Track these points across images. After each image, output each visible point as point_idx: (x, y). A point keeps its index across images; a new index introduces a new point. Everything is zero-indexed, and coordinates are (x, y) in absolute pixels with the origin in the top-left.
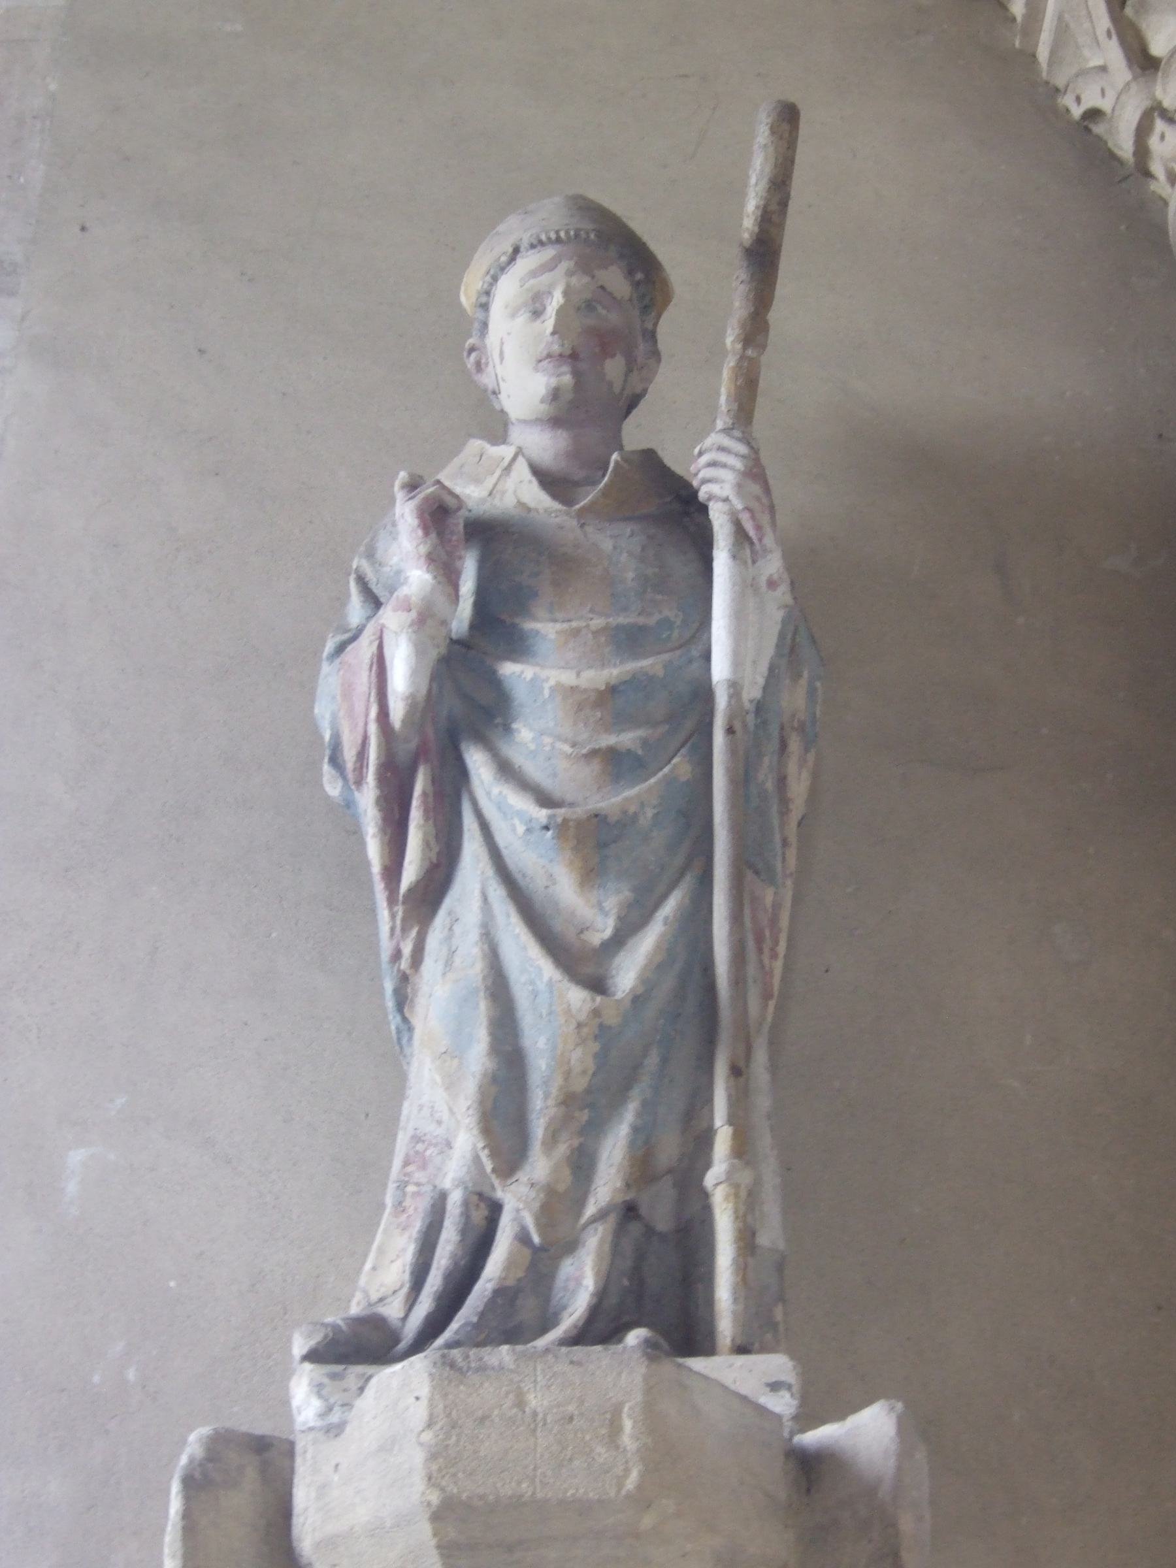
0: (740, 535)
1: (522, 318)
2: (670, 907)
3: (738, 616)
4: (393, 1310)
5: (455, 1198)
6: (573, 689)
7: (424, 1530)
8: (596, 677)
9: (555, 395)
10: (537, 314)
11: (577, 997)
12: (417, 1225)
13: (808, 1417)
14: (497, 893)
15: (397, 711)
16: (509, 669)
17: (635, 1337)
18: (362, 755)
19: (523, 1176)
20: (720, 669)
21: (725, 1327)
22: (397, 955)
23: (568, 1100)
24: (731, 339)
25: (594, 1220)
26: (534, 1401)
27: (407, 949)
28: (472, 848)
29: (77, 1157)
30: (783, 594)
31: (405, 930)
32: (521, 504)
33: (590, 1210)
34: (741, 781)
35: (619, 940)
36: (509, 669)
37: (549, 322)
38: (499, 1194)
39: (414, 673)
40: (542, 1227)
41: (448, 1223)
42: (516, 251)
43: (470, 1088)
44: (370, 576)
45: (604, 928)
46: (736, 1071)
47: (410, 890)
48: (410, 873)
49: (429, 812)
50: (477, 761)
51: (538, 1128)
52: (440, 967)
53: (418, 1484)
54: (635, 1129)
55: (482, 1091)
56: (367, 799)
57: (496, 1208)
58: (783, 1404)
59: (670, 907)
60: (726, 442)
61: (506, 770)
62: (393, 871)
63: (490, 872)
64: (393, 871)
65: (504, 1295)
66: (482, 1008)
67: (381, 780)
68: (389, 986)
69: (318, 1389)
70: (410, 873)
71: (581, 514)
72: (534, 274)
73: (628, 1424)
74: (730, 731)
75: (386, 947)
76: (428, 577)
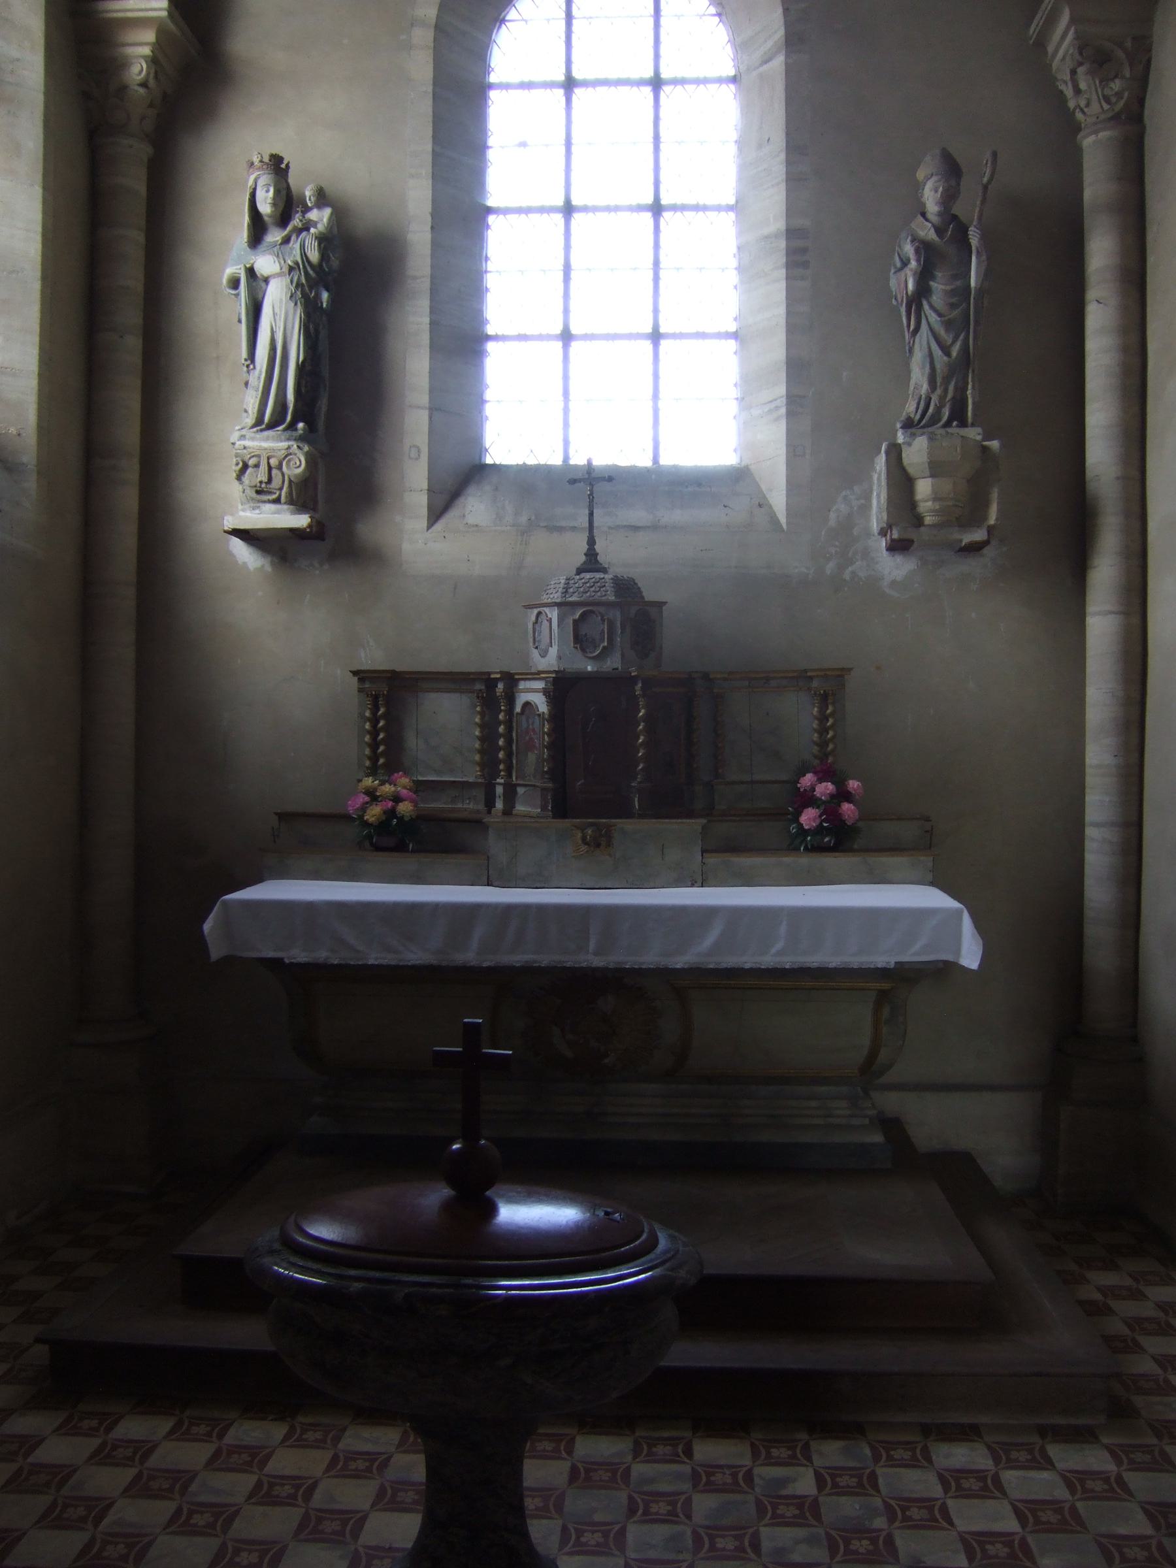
0: (978, 252)
1: (933, 193)
2: (962, 337)
3: (977, 268)
4: (912, 416)
5: (923, 396)
6: (945, 290)
7: (927, 465)
8: (949, 288)
9: (939, 212)
10: (936, 191)
11: (945, 358)
12: (916, 401)
13: (984, 440)
14: (930, 334)
15: (910, 293)
16: (932, 283)
17: (955, 423)
18: (902, 301)
19: (936, 393)
20: (973, 284)
21: (970, 420)
22: (910, 343)
23: (943, 378)
24: (978, 203)
25: (948, 401)
26: (944, 444)
27: (912, 342)
28: (924, 322)
29: (845, 374)
30: (986, 263)
31: (911, 337)
32: (932, 239)
33: (947, 400)
34: (976, 312)
35: (954, 342)
36: (932, 283)
37: (939, 193)
38: (931, 396)
39: (913, 286)
40: (939, 403)
41: (922, 401)
42: (932, 175)
43: (926, 375)
44: (900, 253)
45: (949, 341)
46: (973, 371)
47: (913, 330)
48: (912, 328)
49: (916, 313)
50: (925, 303)
51: (938, 384)
52: (919, 349)
53: (926, 458)
54: (955, 383)
55: (928, 377)
56: (903, 310)
57: (930, 399)
58: (979, 438)
59: (962, 337)
60: (976, 230)
61: (932, 307)
62: (909, 326)
63: (928, 329)
64: (909, 326)
65: (933, 415)
66: (928, 359)
67: (906, 306)
68: (907, 348)
69: (903, 434)
70: (912, 328)
71: (945, 243)
72: (935, 182)
73: (958, 449)
74: (974, 298)
75: (907, 341)
76: (916, 264)
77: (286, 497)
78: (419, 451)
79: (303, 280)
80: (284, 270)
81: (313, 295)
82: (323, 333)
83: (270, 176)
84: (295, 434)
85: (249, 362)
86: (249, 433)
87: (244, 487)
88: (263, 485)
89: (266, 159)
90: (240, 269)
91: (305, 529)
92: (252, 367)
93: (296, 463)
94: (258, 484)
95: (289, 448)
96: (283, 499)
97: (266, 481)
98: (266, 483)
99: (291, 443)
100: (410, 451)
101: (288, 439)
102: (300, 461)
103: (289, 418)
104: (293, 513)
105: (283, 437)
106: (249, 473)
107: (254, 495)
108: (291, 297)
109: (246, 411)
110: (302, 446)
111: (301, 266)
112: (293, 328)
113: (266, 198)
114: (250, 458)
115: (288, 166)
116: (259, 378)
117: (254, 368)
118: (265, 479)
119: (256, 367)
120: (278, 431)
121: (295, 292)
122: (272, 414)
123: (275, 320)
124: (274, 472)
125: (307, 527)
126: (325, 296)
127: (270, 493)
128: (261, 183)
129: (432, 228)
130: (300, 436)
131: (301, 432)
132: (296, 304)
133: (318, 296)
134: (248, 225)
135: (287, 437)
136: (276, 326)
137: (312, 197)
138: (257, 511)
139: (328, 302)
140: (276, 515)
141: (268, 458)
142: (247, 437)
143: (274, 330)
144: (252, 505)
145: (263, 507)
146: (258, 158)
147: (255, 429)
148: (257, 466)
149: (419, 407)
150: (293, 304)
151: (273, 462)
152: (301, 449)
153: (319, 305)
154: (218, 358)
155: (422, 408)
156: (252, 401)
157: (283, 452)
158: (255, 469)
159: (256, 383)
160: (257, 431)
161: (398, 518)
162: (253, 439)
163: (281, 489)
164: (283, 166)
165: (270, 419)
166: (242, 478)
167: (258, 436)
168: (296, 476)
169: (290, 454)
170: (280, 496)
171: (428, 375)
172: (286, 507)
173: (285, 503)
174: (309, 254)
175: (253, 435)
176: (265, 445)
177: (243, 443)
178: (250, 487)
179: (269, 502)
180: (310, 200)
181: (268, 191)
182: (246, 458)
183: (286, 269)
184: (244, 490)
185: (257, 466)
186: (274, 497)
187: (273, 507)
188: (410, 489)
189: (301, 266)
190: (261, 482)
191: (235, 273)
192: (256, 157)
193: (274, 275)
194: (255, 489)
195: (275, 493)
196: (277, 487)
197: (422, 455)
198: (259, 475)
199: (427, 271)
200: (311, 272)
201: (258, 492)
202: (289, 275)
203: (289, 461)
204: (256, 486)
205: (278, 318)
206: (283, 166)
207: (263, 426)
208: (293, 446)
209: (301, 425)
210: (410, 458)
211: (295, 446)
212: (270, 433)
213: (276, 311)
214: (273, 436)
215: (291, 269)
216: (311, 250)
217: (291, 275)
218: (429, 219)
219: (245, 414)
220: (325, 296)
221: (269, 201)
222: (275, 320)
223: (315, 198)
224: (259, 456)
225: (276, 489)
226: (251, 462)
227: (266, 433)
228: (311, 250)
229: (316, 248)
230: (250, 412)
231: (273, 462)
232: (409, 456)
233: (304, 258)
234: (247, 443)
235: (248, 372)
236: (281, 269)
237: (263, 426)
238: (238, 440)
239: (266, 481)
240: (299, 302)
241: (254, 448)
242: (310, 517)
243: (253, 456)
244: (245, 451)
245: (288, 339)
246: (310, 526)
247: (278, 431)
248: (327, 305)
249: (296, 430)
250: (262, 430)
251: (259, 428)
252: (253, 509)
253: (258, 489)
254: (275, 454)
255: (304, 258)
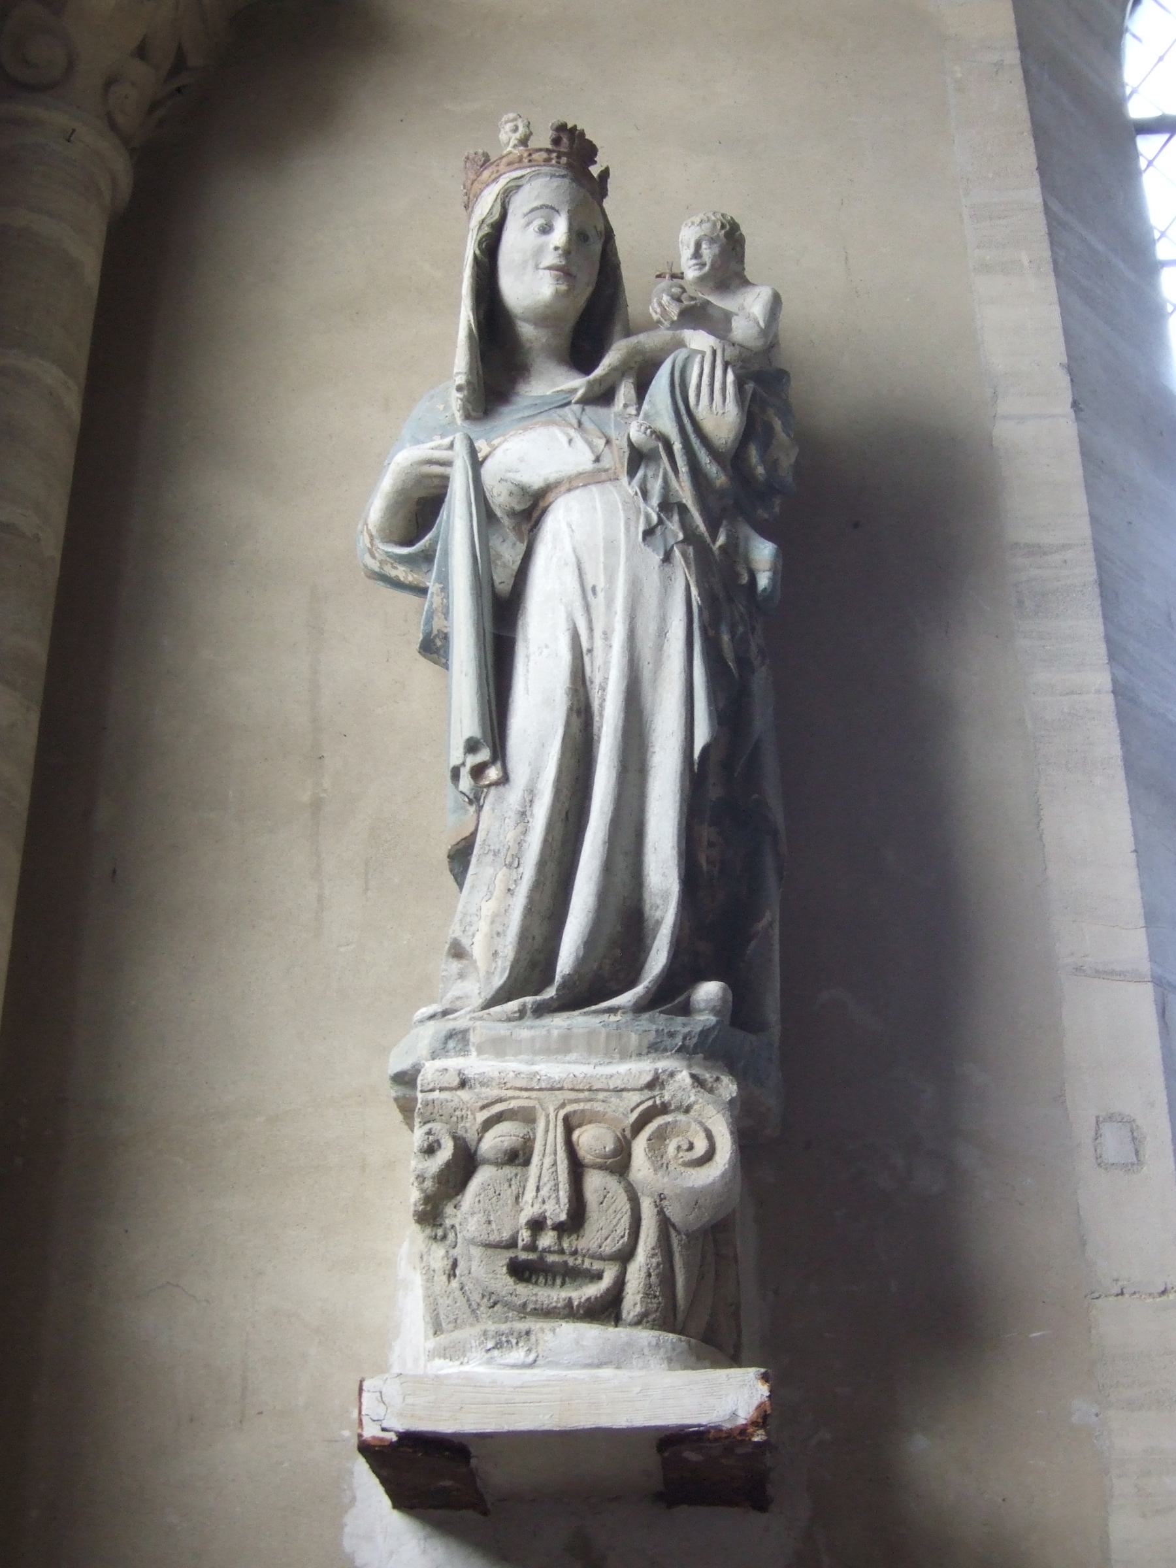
77: (647, 1295)
78: (1136, 1141)
79: (685, 492)
80: (606, 462)
81: (721, 540)
82: (761, 680)
83: (556, 182)
84: (679, 1024)
85: (484, 755)
86: (484, 1028)
87: (455, 1252)
88: (547, 1240)
89: (543, 139)
90: (451, 446)
91: (743, 1430)
92: (493, 773)
93: (691, 1147)
94: (525, 1236)
95: (655, 1083)
96: (633, 1301)
97: (563, 1217)
98: (560, 1228)
99: (665, 1064)
100: (1097, 1135)
101: (655, 1048)
102: (710, 1136)
103: (658, 959)
104: (675, 1361)
105: (634, 1038)
106: (484, 1187)
107: (504, 1283)
108: (649, 533)
109: (458, 952)
110: (707, 1076)
111: (677, 447)
112: (662, 633)
113: (539, 252)
114: (488, 1124)
115: (605, 174)
116: (523, 815)
117: (505, 779)
118: (558, 1211)
119: (512, 776)
120: (612, 1010)
121: (660, 522)
122: (590, 942)
123: (587, 608)
124: (594, 1182)
125: (754, 1423)
126: (763, 552)
127: (573, 1274)
128: (520, 205)
129: (1075, 404)
130: (705, 1033)
131: (705, 1019)
132: (667, 558)
133: (735, 553)
134: (470, 335)
135: (652, 1036)
136: (591, 629)
137: (704, 246)
138: (518, 1355)
139: (774, 570)
140: (606, 1372)
141: (569, 1127)
142: (473, 1038)
143: (585, 645)
144: (492, 1327)
145: (549, 1336)
146: (516, 129)
147: (513, 1005)
148: (518, 1156)
149: (1113, 973)
150: (657, 558)
151: (590, 1140)
152: (711, 1091)
153: (745, 579)
154: (317, 805)
155: (1139, 980)
156: (489, 908)
157: (635, 1097)
158: (508, 1171)
159: (511, 835)
160: (522, 1013)
161: (1082, 1410)
162: (498, 1047)
163: (625, 1256)
164: (595, 170)
165: (581, 963)
166: (449, 1209)
167: (527, 1031)
168: (695, 1198)
169: (664, 1109)
170: (620, 1284)
171: (1132, 858)
172: (645, 1336)
173: (638, 1322)
174: (702, 411)
175: (503, 1029)
176: (553, 1070)
177: (454, 1063)
178: (488, 1246)
179: (571, 1312)
180: (697, 254)
181: (546, 229)
182: (470, 1127)
183: (616, 459)
184: (455, 1264)
185: (518, 1156)
186: (593, 1290)
187: (592, 1334)
188: (1117, 1290)
189: (677, 447)
190: (537, 1225)
191: (430, 462)
192: (509, 126)
193: (570, 479)
194: (505, 1256)
195: (599, 1276)
196: (609, 1248)
197: (1148, 1150)
198: (530, 1194)
199: (1083, 529)
200: (711, 468)
201: (520, 1271)
202: (632, 473)
203: (660, 1137)
204: (512, 1244)
205: (599, 603)
206: (595, 170)
207: (550, 993)
208: (672, 1075)
209: (709, 991)
210: (1100, 1162)
211: (684, 1077)
212: (578, 1021)
213: (590, 581)
214: (591, 1034)
215: (637, 458)
216: (712, 399)
217: (640, 474)
218: (1064, 380)
219: (455, 966)
220: (763, 552)
221: (551, 258)
222: (587, 608)
223: (716, 249)
224: (526, 1116)
225: (602, 1258)
226: (493, 1142)
227: (559, 1022)
228: (712, 399)
229: (730, 389)
230: (478, 949)
231: (590, 1140)
232: (1098, 1157)
233: (686, 420)
234: (474, 1064)
235: (476, 800)
236: (597, 460)
237: (550, 993)
238: (434, 1056)
239: (563, 1217)
240: (677, 553)
241: (503, 1084)
242: (765, 1378)
243: (498, 1118)
244: (464, 1094)
245: (646, 674)
246: (763, 1419)
247: (612, 1010)
248: (773, 580)
249: (686, 1010)
250: (541, 1010)
251: (529, 1000)
252: (498, 1346)
253: (523, 1256)
254: (598, 1107)
255: (686, 420)
